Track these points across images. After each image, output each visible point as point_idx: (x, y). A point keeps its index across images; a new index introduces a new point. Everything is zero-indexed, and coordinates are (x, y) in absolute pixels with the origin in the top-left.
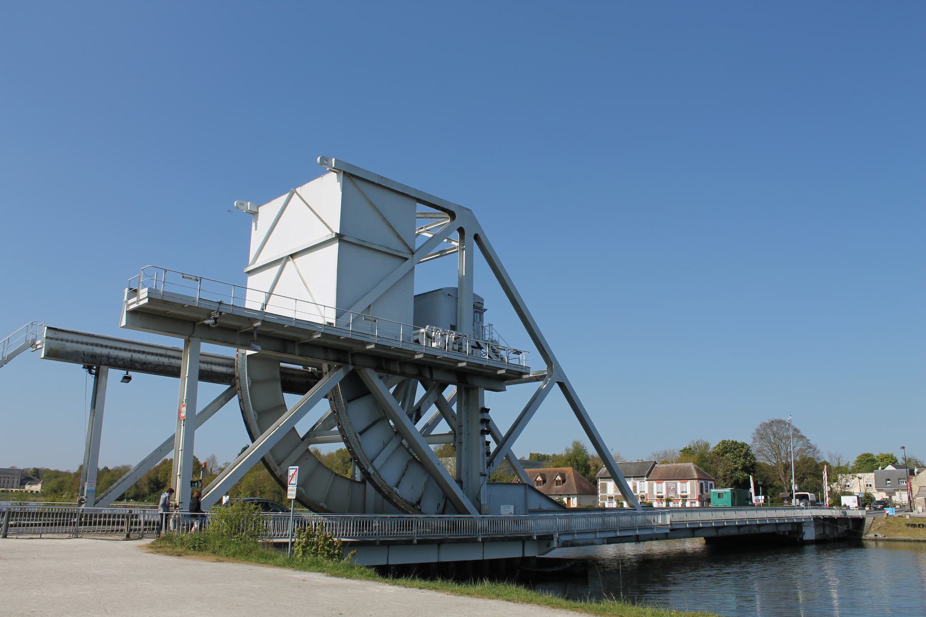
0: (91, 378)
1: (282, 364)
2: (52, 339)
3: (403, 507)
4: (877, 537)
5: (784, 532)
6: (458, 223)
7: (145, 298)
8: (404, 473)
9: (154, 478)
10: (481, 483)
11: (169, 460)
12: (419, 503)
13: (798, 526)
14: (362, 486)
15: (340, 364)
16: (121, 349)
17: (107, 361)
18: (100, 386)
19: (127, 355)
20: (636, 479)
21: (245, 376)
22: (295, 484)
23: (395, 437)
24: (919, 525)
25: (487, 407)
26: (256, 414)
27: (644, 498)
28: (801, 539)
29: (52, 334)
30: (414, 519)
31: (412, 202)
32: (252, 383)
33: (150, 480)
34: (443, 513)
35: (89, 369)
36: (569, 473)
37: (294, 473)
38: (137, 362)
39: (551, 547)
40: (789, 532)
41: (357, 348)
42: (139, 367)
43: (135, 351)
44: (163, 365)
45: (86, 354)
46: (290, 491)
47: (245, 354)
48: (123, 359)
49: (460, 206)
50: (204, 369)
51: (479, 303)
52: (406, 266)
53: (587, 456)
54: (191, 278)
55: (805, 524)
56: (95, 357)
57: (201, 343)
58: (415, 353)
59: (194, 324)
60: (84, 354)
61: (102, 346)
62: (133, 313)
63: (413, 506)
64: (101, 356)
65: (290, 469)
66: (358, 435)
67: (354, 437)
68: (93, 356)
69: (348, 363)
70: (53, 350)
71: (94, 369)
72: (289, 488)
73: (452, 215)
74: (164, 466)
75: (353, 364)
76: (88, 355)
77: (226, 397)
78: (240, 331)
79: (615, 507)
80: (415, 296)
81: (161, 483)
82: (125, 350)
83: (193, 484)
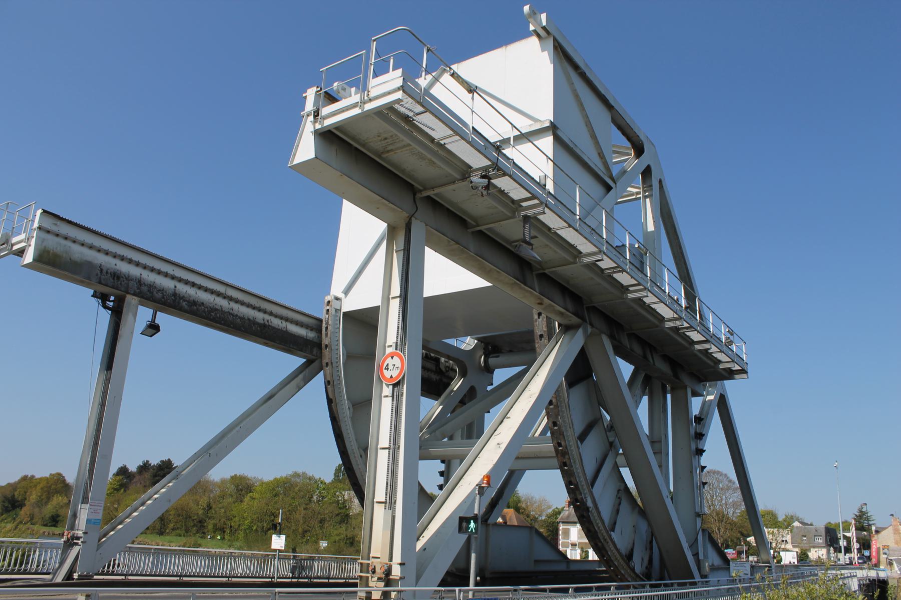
0: (106, 316)
2: (48, 232)
3: (623, 572)
6: (645, 160)
9: (9, 496)
11: (29, 476)
16: (159, 272)
18: (123, 331)
19: (168, 284)
21: (338, 345)
29: (49, 224)
32: (348, 357)
33: (4, 497)
35: (103, 298)
36: (510, 515)
38: (183, 298)
42: (186, 307)
43: (180, 280)
44: (220, 311)
45: (105, 271)
47: (340, 310)
48: (162, 290)
50: (277, 327)
53: (518, 498)
59: (414, 195)
60: (101, 270)
61: (130, 261)
64: (128, 278)
68: (116, 276)
69: (586, 322)
70: (48, 252)
71: (111, 301)
74: (23, 483)
76: (107, 273)
77: (303, 375)
79: (578, 558)
81: (18, 501)
82: (166, 275)
83: (464, 524)
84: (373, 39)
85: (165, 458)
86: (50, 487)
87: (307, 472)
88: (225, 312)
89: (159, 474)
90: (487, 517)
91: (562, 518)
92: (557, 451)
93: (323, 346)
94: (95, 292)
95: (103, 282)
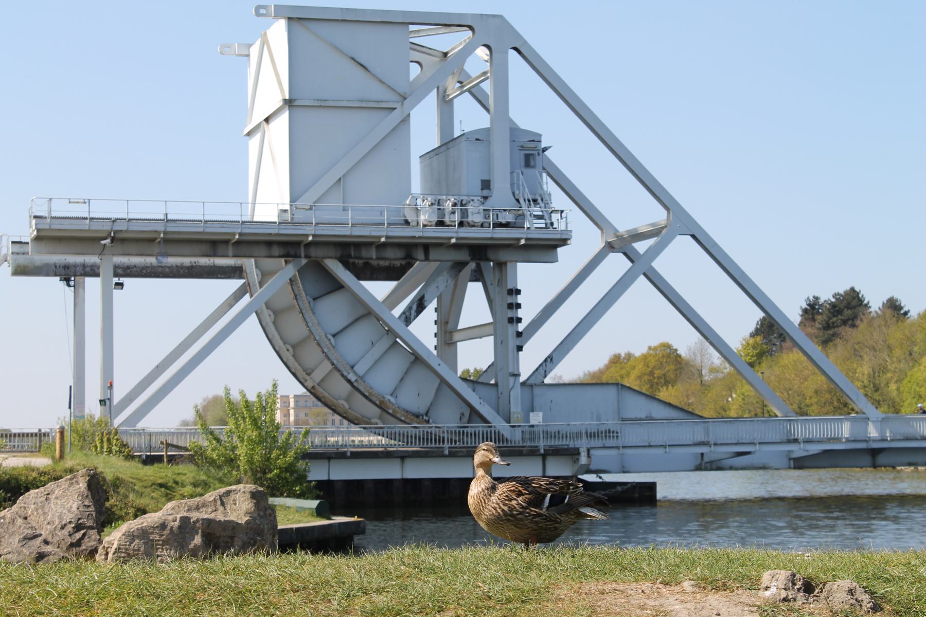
2: (18, 254)
10: (511, 386)
17: (83, 270)
23: (386, 335)
25: (519, 288)
31: (398, 30)
35: (67, 280)
45: (58, 266)
50: (204, 265)
51: (533, 141)
52: (396, 116)
54: (78, 202)
56: (68, 268)
60: (56, 266)
64: (75, 266)
67: (326, 340)
68: (66, 267)
70: (20, 266)
75: (306, 257)
76: (60, 267)
86: (651, 373)
87: (751, 332)
88: (155, 267)
89: (833, 323)
90: (333, 456)
94: (61, 278)
95: (57, 274)
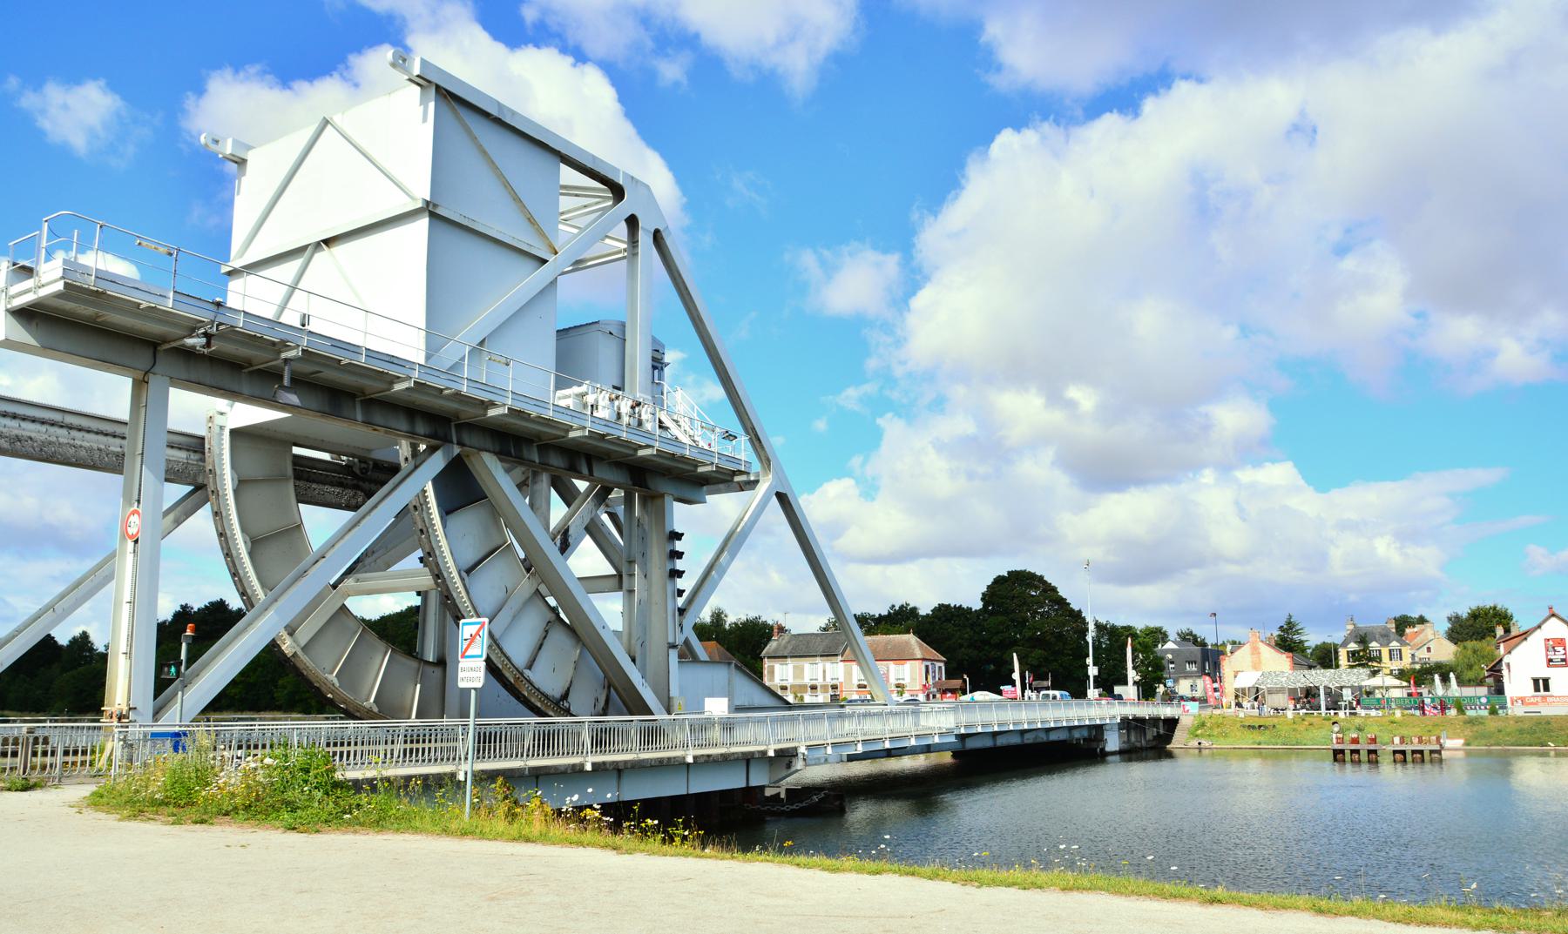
1: (297, 450)
4: (1202, 746)
5: (1078, 739)
7: (56, 281)
8: (541, 645)
12: (565, 696)
13: (1098, 730)
14: (438, 671)
15: (434, 442)
20: (825, 658)
22: (481, 656)
24: (1260, 726)
26: (248, 539)
27: (837, 688)
28: (1103, 750)
30: (616, 724)
34: (605, 714)
37: (478, 633)
39: (793, 769)
40: (1084, 740)
41: (469, 413)
46: (464, 670)
49: (632, 178)
55: (1107, 727)
57: (170, 388)
58: (570, 428)
59: (155, 348)
62: (26, 315)
63: (557, 704)
65: (464, 624)
66: (464, 574)
69: (452, 442)
72: (460, 665)
73: (618, 192)
75: (460, 443)
78: (251, 369)
80: (558, 331)
84: (45, 219)
85: (215, 598)
91: (767, 653)
92: (436, 583)
93: (207, 471)
